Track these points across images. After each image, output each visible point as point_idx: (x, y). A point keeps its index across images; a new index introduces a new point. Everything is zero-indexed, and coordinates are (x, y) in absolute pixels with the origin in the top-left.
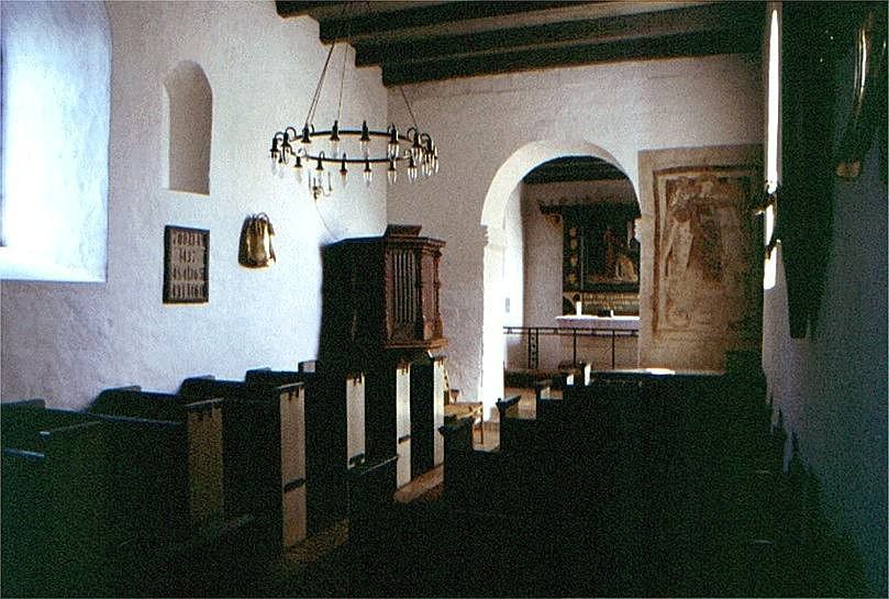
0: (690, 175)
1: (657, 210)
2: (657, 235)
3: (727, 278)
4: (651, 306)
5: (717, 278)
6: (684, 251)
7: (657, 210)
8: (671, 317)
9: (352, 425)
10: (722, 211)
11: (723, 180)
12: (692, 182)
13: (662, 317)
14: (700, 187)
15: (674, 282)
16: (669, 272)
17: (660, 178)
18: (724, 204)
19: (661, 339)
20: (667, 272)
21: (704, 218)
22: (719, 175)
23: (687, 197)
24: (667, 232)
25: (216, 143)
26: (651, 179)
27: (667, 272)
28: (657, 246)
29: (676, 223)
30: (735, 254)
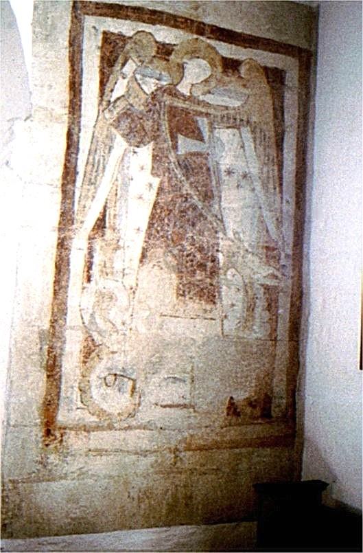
0: (164, 34)
1: (75, 106)
2: (69, 173)
3: (230, 296)
4: (7, 367)
5: (210, 295)
6: (133, 219)
7: (75, 106)
8: (95, 393)
9: (356, 346)
10: (225, 135)
11: (231, 66)
12: (165, 51)
13: (70, 390)
14: (181, 67)
15: (106, 297)
16: (95, 271)
17: (90, 21)
18: (233, 121)
19: (65, 455)
20: (89, 266)
21: (185, 145)
22: (226, 50)
23: (150, 86)
24: (97, 167)
25: (360, 161)
26: (67, 23)
27: (89, 266)
28: (67, 195)
29: (120, 144)
30: (249, 237)
